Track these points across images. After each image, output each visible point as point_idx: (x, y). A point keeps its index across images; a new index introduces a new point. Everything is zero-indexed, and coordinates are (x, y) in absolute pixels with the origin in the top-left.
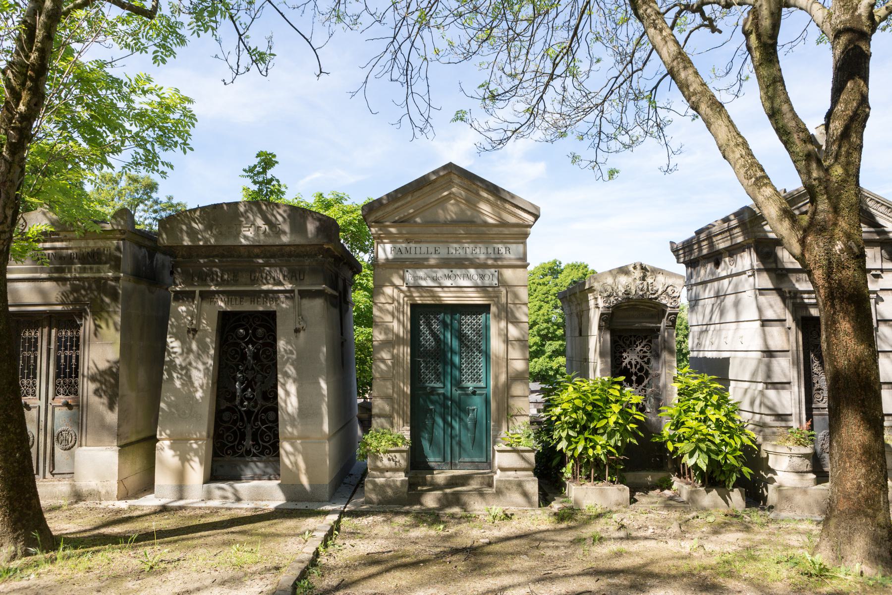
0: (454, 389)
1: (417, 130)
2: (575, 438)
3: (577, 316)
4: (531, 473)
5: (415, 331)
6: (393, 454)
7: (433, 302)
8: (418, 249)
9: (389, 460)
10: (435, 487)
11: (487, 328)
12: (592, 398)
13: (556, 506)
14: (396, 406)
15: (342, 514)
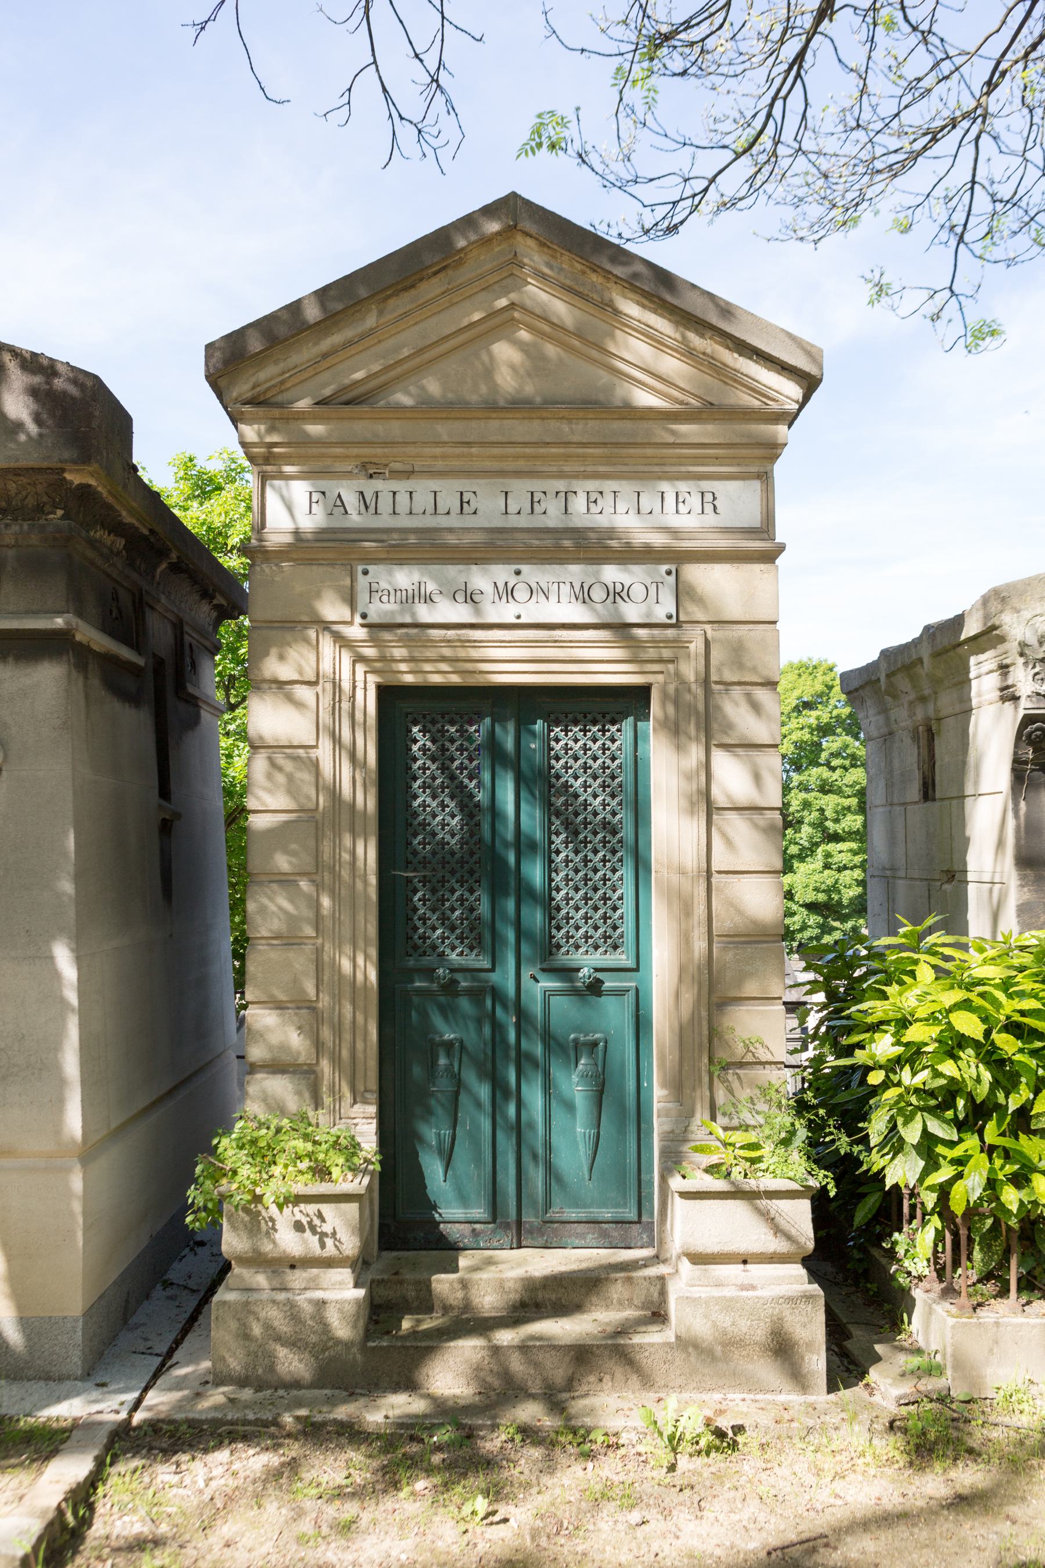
0: (526, 975)
1: (407, 134)
2: (951, 1144)
3: (915, 737)
4: (799, 1271)
5: (392, 774)
6: (311, 1208)
7: (455, 679)
8: (403, 499)
9: (299, 1227)
10: (468, 1323)
11: (639, 767)
12: (1009, 1007)
13: (887, 1386)
14: (326, 1033)
15: (125, 1441)
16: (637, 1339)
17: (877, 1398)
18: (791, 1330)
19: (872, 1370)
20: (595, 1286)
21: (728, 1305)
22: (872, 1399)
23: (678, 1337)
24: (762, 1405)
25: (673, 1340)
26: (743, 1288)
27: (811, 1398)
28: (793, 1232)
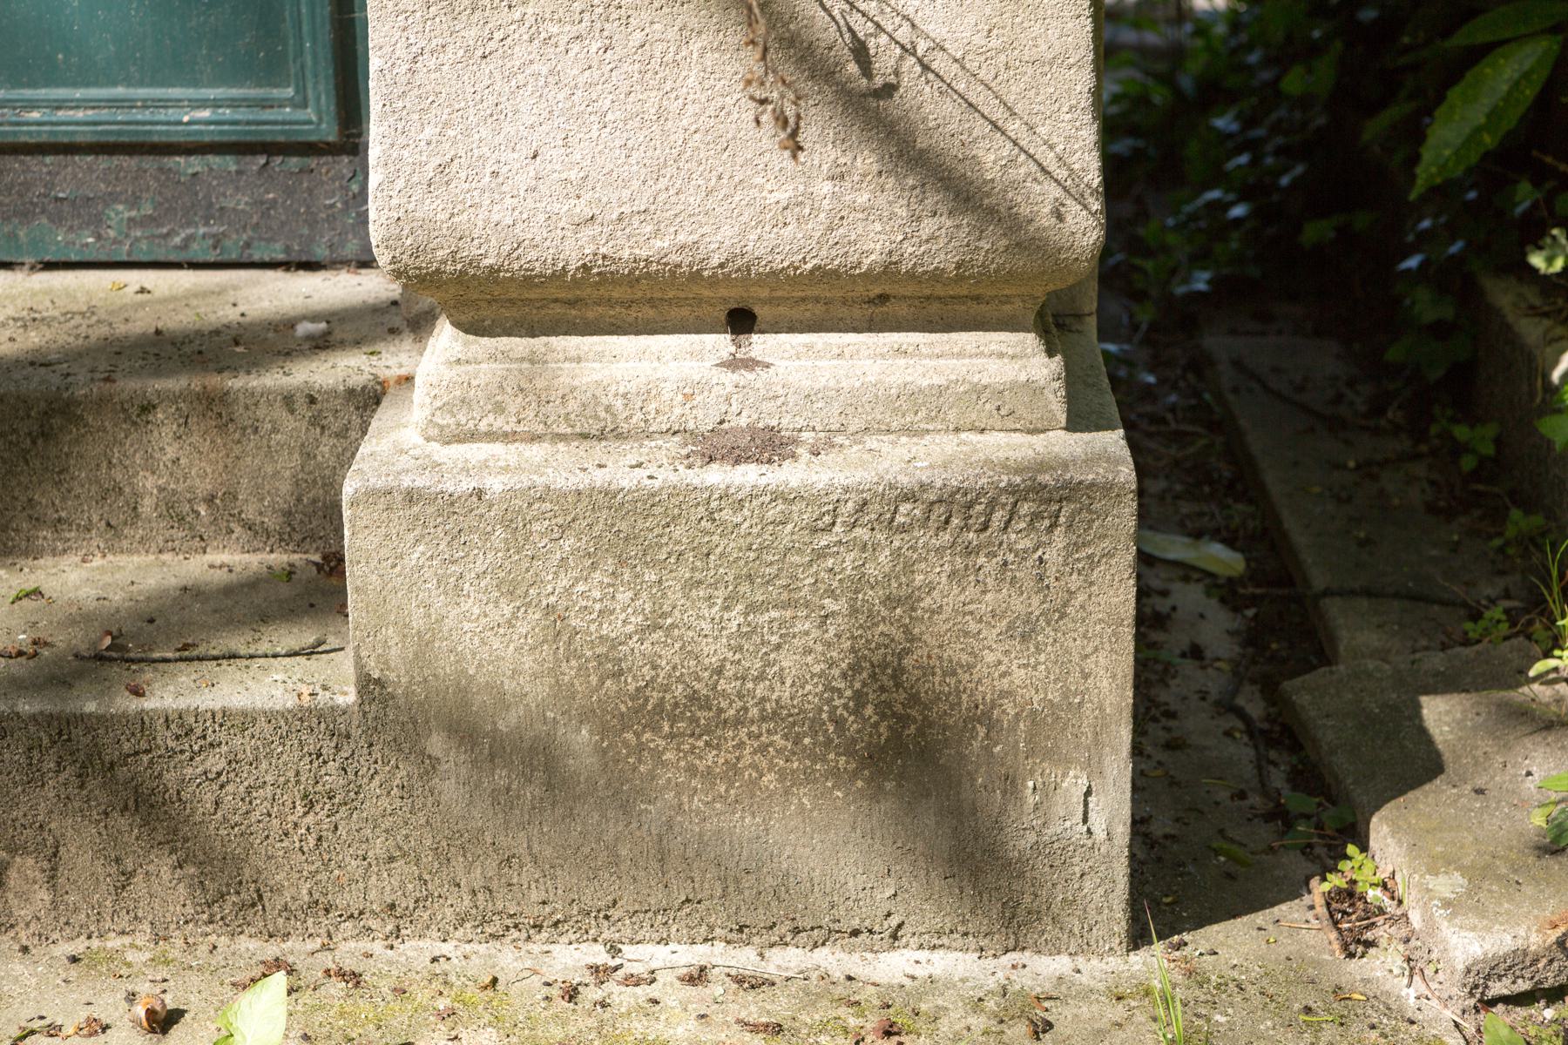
16: (173, 694)
17: (1381, 967)
18: (955, 652)
19: (1380, 829)
20: (46, 434)
21: (623, 530)
22: (1355, 969)
23: (369, 686)
24: (777, 1006)
25: (348, 697)
26: (719, 446)
27: (1043, 968)
28: (991, 157)
